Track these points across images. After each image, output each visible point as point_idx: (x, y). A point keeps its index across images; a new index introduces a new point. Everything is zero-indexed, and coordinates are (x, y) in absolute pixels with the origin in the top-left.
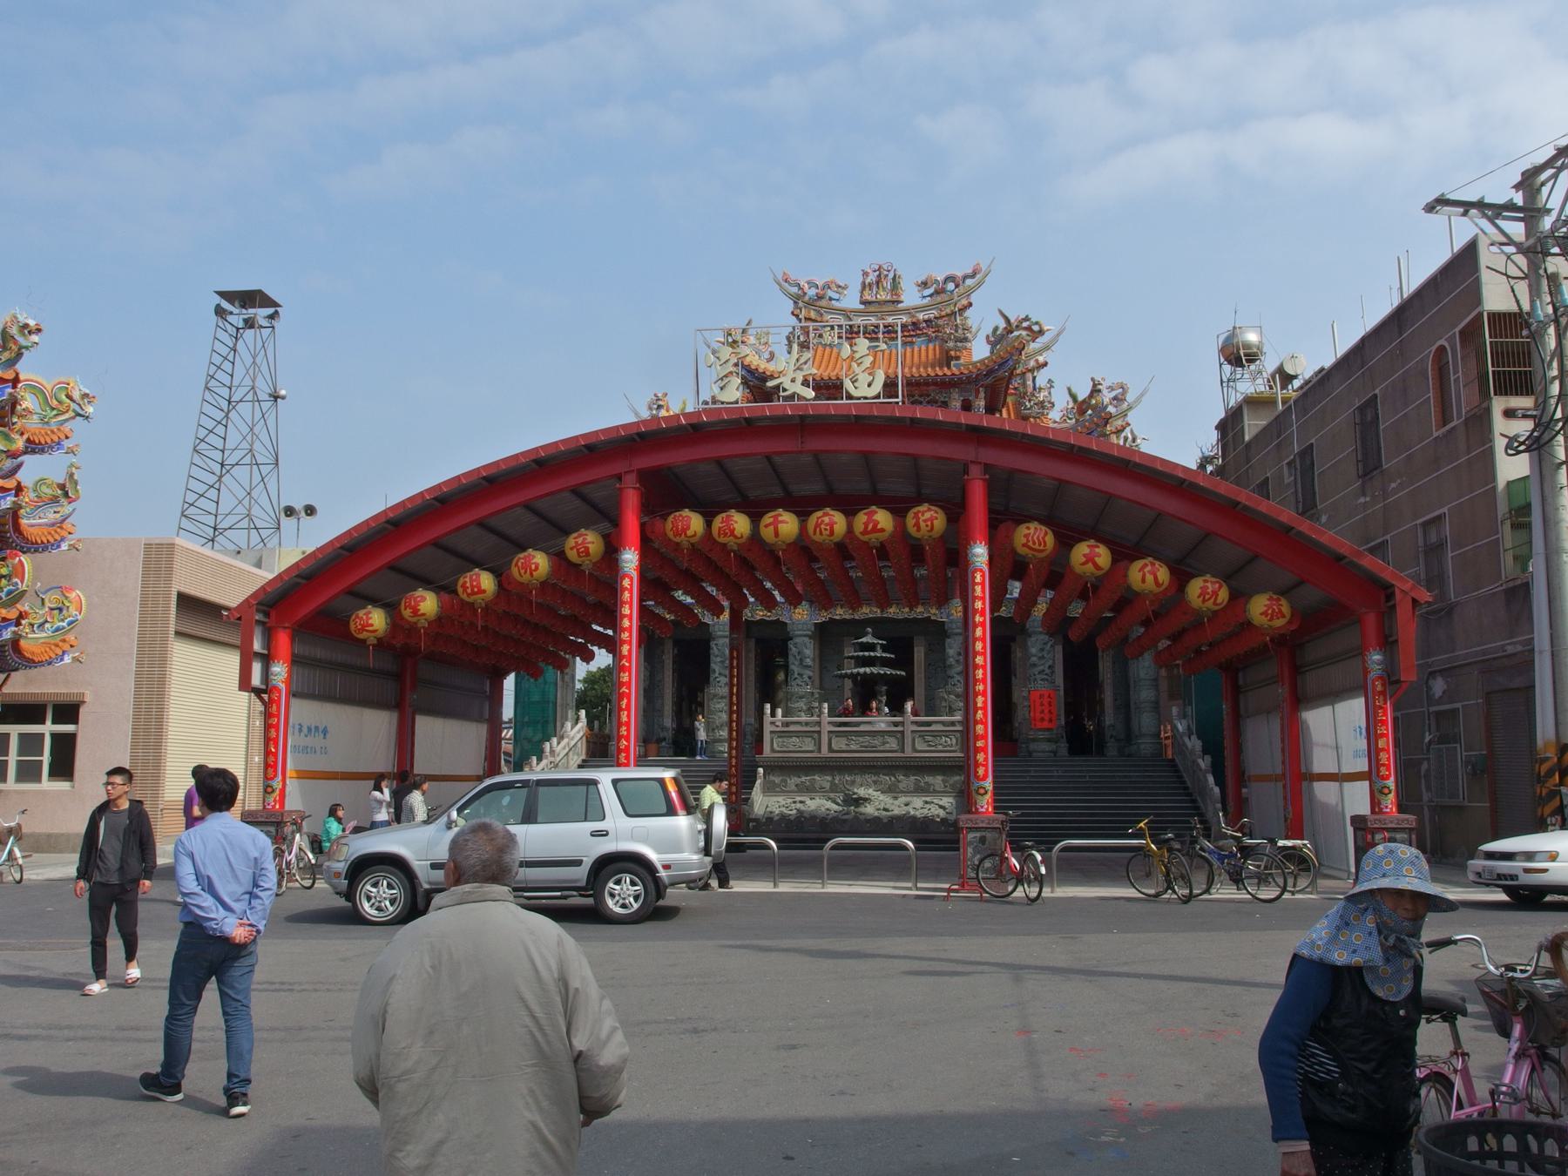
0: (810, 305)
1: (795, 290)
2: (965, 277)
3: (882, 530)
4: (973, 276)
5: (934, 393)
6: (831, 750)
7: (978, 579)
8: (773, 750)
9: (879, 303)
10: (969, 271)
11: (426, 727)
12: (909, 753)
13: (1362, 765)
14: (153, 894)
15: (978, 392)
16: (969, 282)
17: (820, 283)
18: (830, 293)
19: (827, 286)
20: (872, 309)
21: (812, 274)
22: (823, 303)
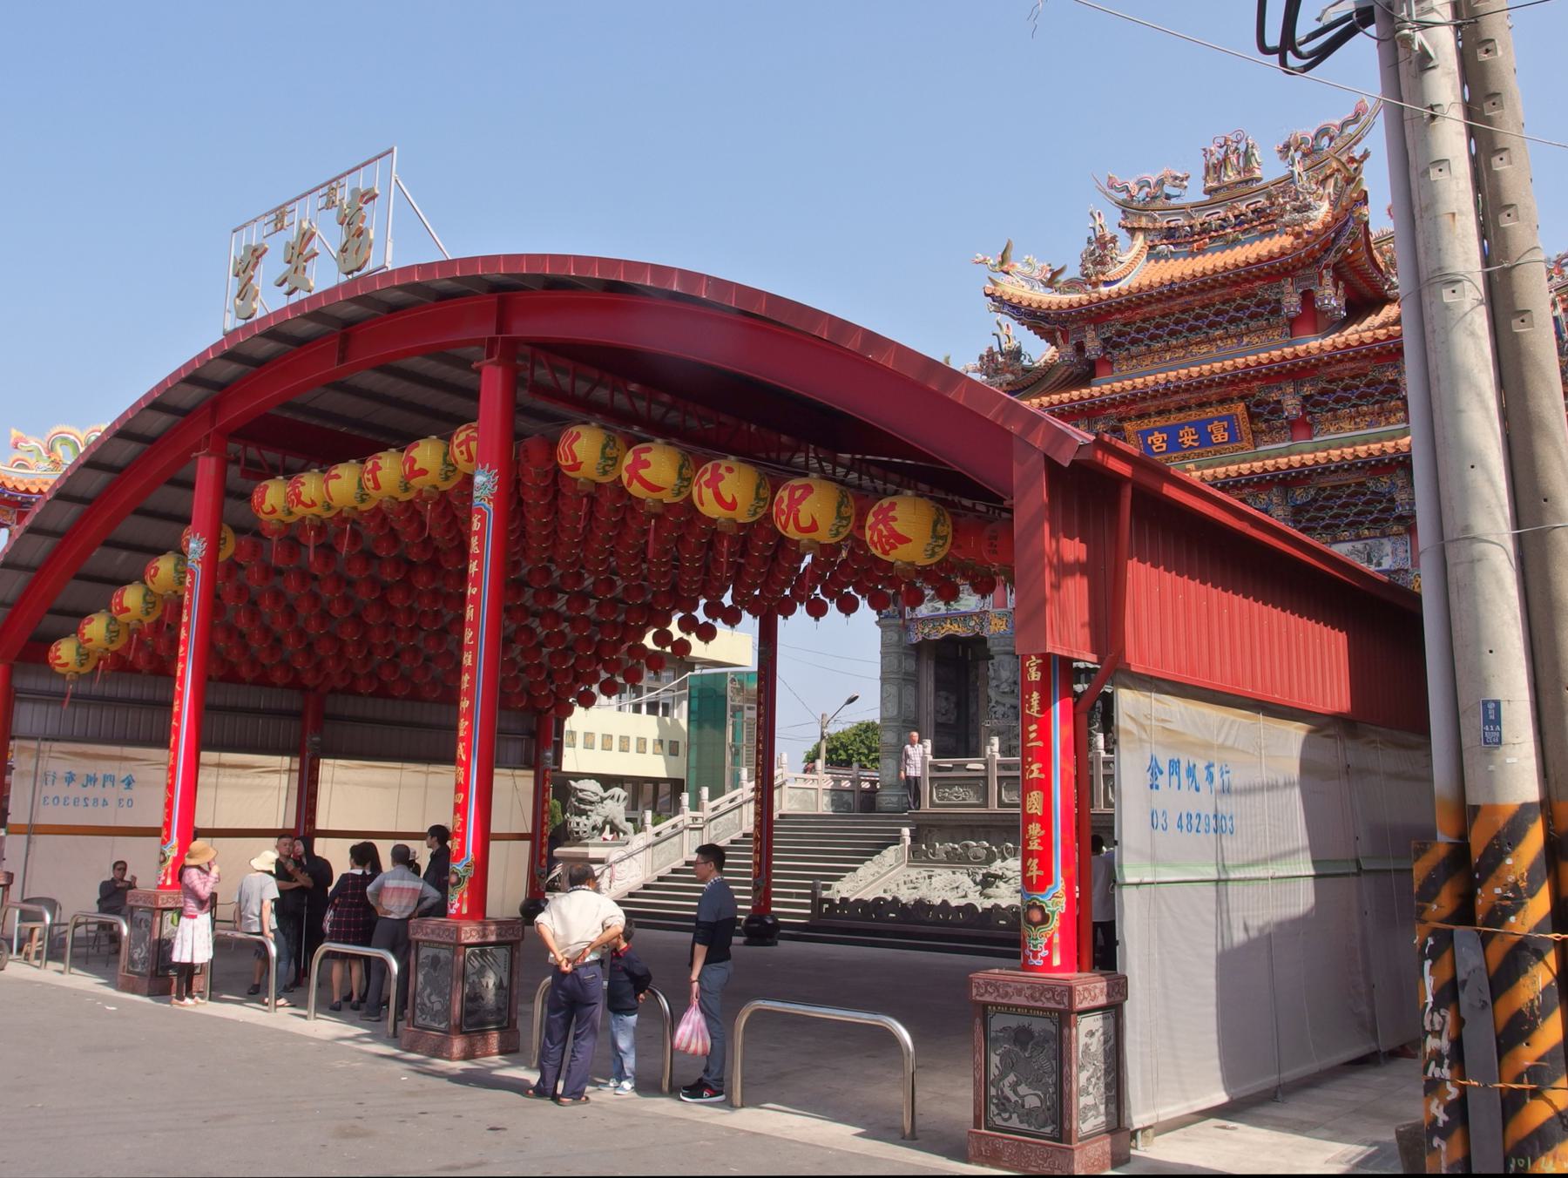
0: (1137, 210)
1: (1124, 196)
2: (1345, 124)
3: (423, 472)
4: (1355, 119)
5: (1261, 289)
6: (1001, 804)
7: (476, 526)
8: (932, 804)
9: (1228, 187)
10: (1349, 115)
11: (331, 771)
12: (994, 807)
13: (494, 846)
14: (187, 950)
15: (1321, 277)
16: (1351, 129)
17: (1153, 181)
18: (1168, 189)
19: (1161, 183)
20: (1219, 197)
21: (1137, 173)
22: (1158, 204)
